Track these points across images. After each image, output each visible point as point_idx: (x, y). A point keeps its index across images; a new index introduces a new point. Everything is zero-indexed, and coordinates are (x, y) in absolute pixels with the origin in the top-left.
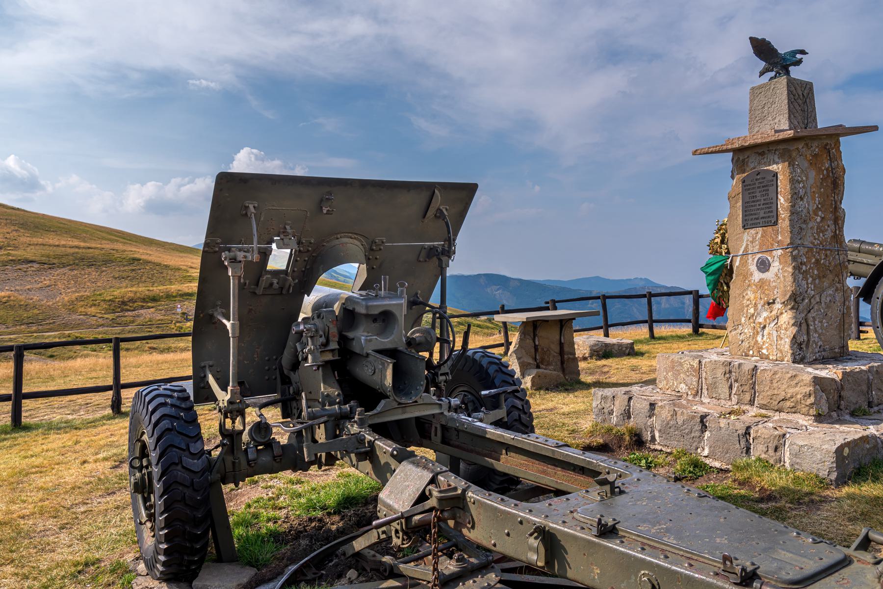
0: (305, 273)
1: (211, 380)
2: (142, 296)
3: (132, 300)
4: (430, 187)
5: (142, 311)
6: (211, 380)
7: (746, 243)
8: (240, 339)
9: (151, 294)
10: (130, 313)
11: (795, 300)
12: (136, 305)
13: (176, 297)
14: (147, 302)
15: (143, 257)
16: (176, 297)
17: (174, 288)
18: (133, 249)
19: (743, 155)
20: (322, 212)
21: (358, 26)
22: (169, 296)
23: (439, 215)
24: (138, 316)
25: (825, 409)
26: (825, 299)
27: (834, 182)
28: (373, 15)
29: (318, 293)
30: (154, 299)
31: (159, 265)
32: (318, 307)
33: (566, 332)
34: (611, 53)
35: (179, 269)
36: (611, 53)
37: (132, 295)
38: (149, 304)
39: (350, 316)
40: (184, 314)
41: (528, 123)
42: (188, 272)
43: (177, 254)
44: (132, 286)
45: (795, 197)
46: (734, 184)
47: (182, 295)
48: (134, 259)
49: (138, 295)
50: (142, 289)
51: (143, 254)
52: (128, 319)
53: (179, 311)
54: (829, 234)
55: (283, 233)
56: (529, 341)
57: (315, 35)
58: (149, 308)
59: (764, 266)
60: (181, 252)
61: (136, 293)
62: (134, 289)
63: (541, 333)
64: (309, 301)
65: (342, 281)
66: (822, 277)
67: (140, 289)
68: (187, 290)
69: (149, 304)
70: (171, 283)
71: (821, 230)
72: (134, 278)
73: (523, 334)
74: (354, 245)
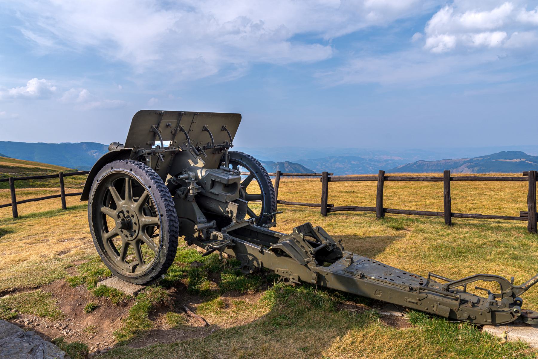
41: (111, 44)
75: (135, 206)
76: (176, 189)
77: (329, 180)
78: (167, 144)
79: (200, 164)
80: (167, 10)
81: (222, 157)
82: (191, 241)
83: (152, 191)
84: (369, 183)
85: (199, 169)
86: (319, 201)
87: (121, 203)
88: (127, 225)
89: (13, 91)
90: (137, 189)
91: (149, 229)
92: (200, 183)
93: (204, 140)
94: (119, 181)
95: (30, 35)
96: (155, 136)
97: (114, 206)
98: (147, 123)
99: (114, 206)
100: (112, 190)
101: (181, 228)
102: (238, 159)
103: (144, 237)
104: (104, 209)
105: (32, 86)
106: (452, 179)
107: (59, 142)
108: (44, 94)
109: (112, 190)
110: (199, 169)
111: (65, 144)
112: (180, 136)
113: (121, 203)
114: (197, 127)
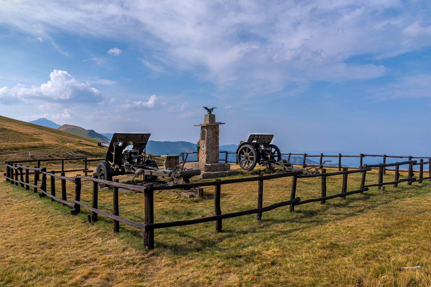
0: (124, 146)
1: (109, 162)
2: (10, 147)
3: (5, 149)
4: (143, 134)
5: (10, 155)
6: (109, 162)
7: (202, 142)
8: (115, 156)
9: (15, 146)
10: (4, 155)
11: (207, 153)
12: (7, 151)
13: (27, 148)
14: (13, 150)
15: (8, 128)
16: (27, 148)
17: (26, 144)
18: (3, 124)
19: (203, 127)
20: (126, 138)
21: (113, 10)
22: (24, 148)
23: (145, 138)
24: (8, 157)
25: (207, 170)
26: (213, 153)
27: (216, 133)
28: (122, 5)
29: (126, 149)
30: (16, 149)
31: (17, 132)
32: (125, 152)
33: (177, 160)
34: (243, 35)
35: (28, 135)
36: (243, 35)
37: (5, 147)
38: (14, 151)
39: (131, 153)
40: (32, 156)
41: (202, 68)
42: (32, 136)
43: (25, 127)
44: (4, 142)
45: (208, 135)
46: (200, 132)
47: (30, 147)
48: (4, 129)
49: (8, 147)
50: (10, 144)
51: (8, 126)
52: (4, 158)
53: (30, 155)
54: (215, 142)
55: (121, 141)
56: (168, 161)
57: (90, 12)
58: (14, 153)
59: (203, 147)
60: (27, 126)
61: (7, 146)
62: (6, 144)
63: (171, 160)
64: (124, 150)
65: (130, 148)
66: (213, 149)
67: (9, 144)
68: (33, 145)
69: (14, 151)
70: (24, 141)
71: (213, 141)
72: (5, 138)
73: (167, 159)
74: (131, 143)
75: (248, 154)
76: (257, 151)
77: (306, 156)
78: (256, 141)
79: (263, 146)
80: (244, 42)
81: (267, 145)
82: (260, 164)
83: (252, 150)
84: (387, 181)
85: (262, 147)
86: (302, 164)
87: (245, 154)
88: (247, 158)
89: (138, 103)
90: (249, 150)
91: (252, 159)
92: (262, 151)
93: (264, 141)
94: (245, 149)
95: (147, 64)
96: (253, 139)
97: (243, 154)
98: (252, 137)
99: (243, 154)
100: (244, 151)
101: (258, 161)
102: (273, 146)
103: (250, 160)
104: (241, 155)
105: (151, 101)
106: (342, 156)
107: (163, 141)
108: (157, 106)
109: (244, 151)
110: (262, 147)
111: (167, 142)
112: (259, 140)
113: (245, 154)
114: (262, 138)
